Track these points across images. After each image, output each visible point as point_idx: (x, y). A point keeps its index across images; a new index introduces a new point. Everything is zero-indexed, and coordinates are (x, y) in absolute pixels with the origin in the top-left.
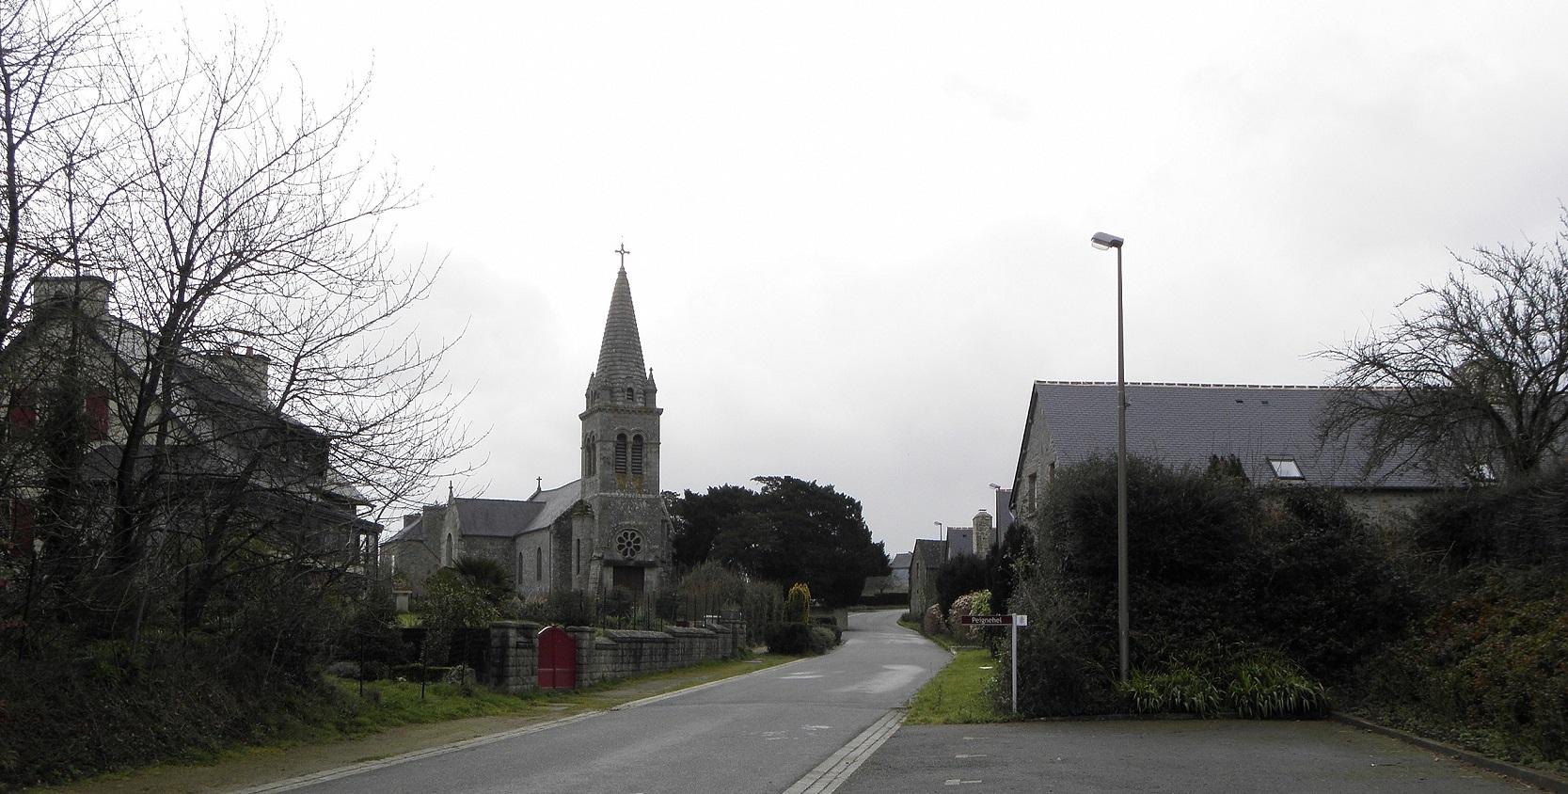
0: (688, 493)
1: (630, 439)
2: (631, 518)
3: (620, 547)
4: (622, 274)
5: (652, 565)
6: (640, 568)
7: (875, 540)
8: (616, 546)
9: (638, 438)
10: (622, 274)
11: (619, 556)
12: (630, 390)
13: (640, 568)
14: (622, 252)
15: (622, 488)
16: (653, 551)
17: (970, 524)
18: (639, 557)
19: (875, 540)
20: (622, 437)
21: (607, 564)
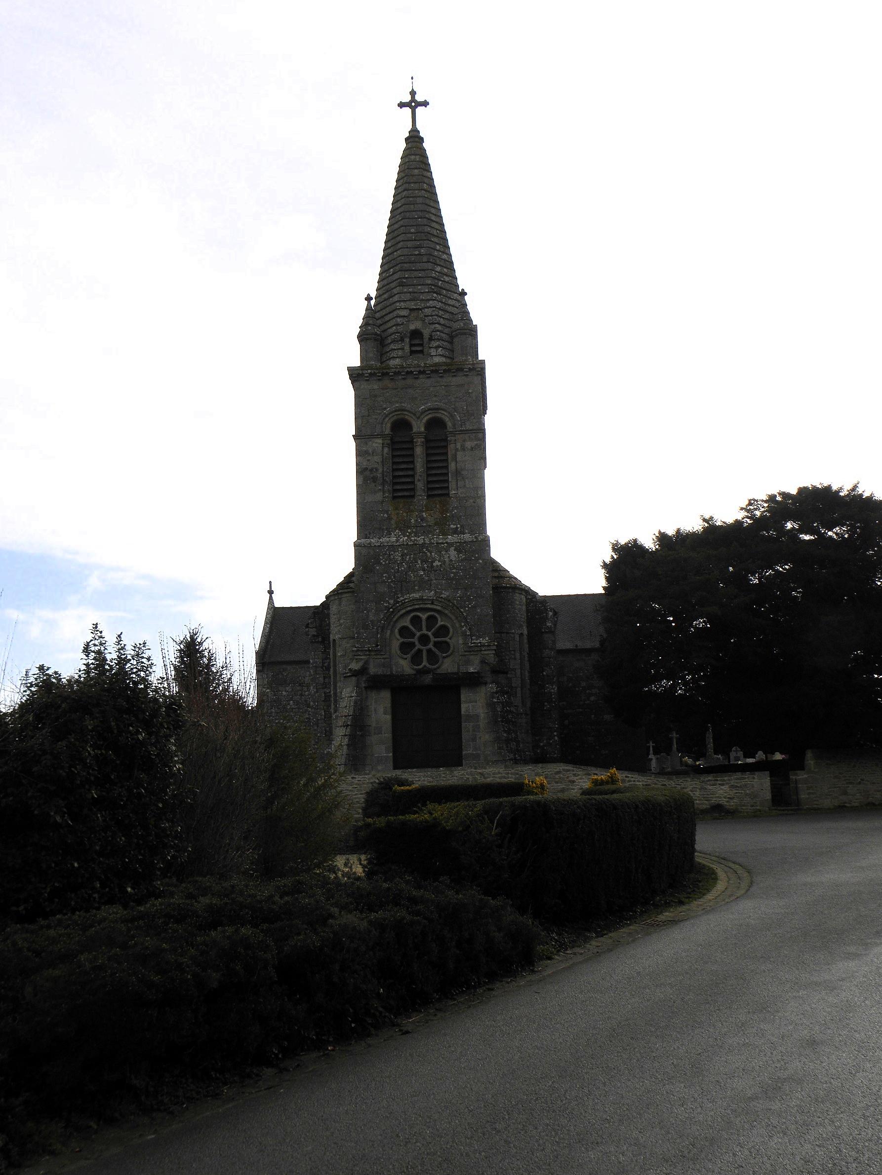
0: (662, 538)
1: (418, 426)
2: (423, 584)
3: (405, 648)
4: (414, 140)
5: (474, 681)
6: (452, 687)
7: (794, 492)
8: (396, 644)
9: (435, 424)
10: (414, 140)
11: (404, 666)
12: (416, 334)
13: (452, 687)
14: (413, 104)
15: (403, 526)
16: (477, 649)
17: (480, 358)
18: (448, 666)
19: (794, 492)
20: (401, 425)
21: (376, 683)
